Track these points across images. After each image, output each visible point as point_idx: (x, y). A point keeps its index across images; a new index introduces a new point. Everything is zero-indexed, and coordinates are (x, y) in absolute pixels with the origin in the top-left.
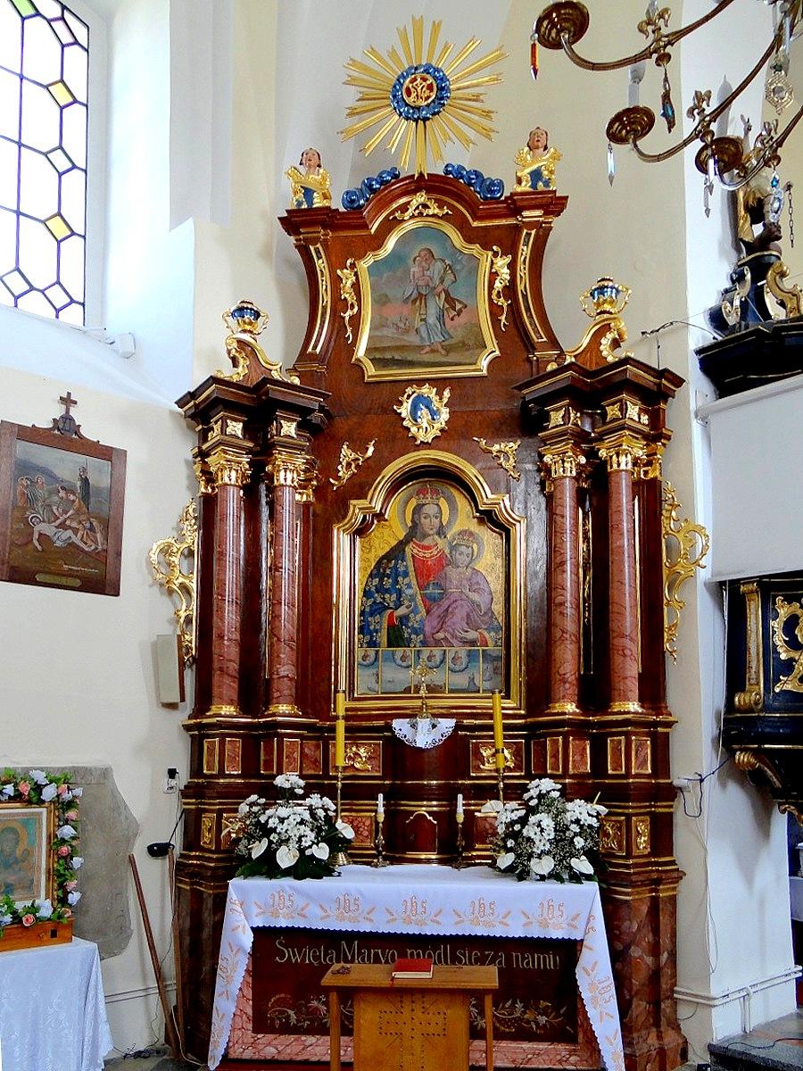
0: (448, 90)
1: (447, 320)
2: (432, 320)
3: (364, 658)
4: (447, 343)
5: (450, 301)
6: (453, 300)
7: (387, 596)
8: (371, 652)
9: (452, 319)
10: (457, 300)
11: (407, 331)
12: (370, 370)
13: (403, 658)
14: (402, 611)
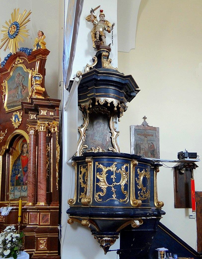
0: (18, 24)
1: (22, 92)
2: (19, 93)
3: (12, 188)
4: (22, 98)
5: (23, 86)
6: (24, 86)
7: (16, 171)
8: (13, 187)
9: (23, 92)
10: (25, 86)
11: (14, 97)
12: (7, 110)
13: (19, 189)
14: (19, 175)
